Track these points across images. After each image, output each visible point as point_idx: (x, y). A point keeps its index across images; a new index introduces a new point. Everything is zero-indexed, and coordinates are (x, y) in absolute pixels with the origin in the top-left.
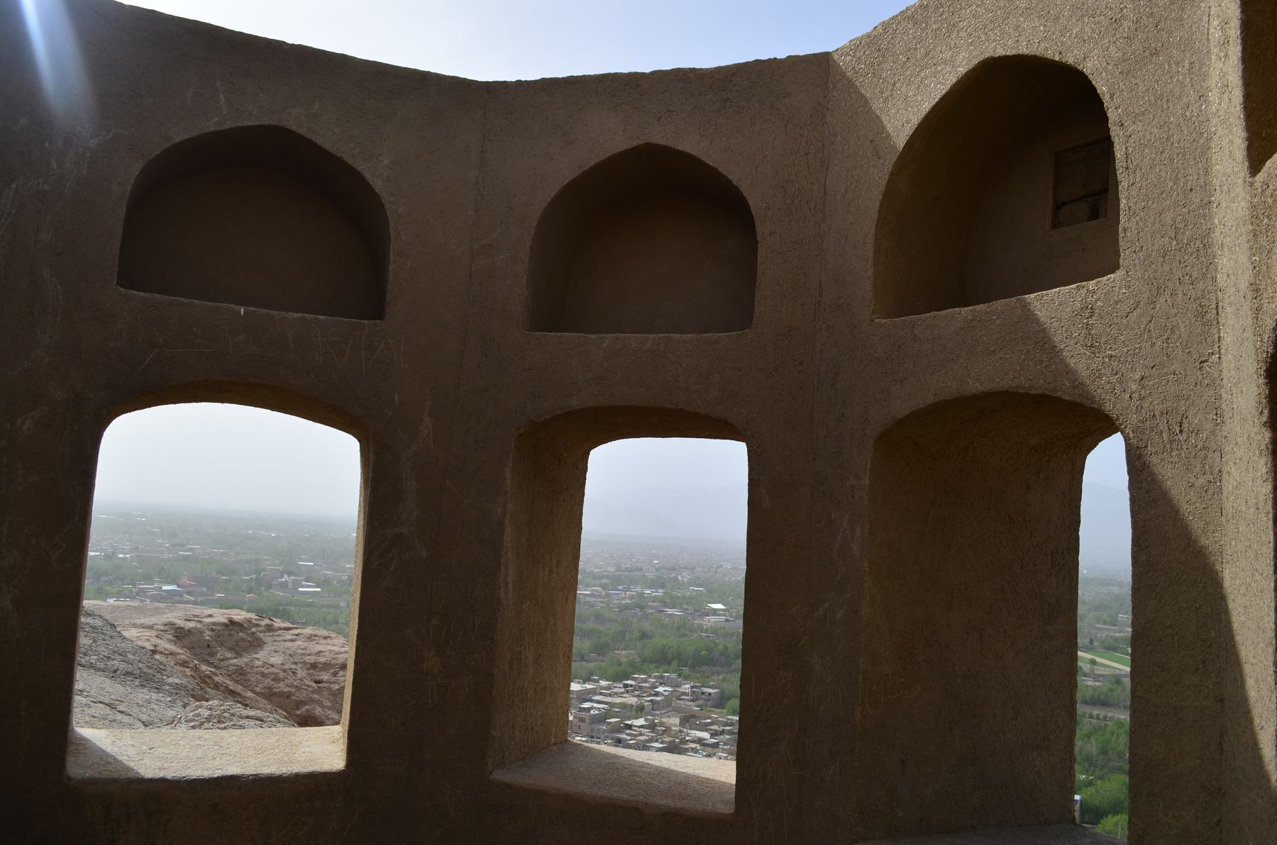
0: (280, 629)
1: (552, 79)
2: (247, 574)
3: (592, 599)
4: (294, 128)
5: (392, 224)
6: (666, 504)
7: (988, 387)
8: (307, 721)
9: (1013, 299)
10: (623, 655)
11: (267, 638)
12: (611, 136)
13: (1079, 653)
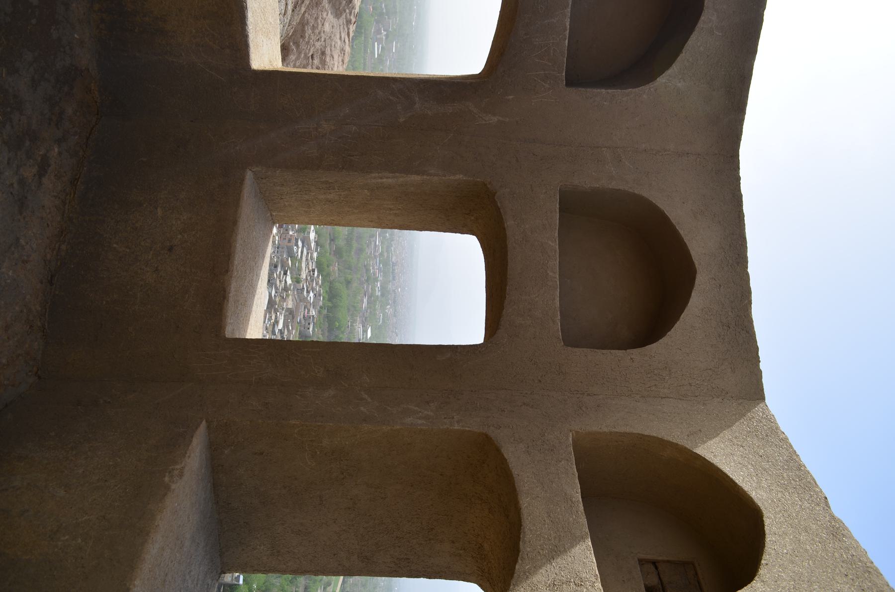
0: (348, 29)
1: (742, 201)
2: (386, 6)
3: (373, 246)
4: (702, 18)
5: (634, 90)
6: (439, 289)
7: (525, 512)
8: (285, 50)
9: (587, 530)
10: (335, 268)
11: (342, 20)
12: (700, 243)
13: (342, 577)
